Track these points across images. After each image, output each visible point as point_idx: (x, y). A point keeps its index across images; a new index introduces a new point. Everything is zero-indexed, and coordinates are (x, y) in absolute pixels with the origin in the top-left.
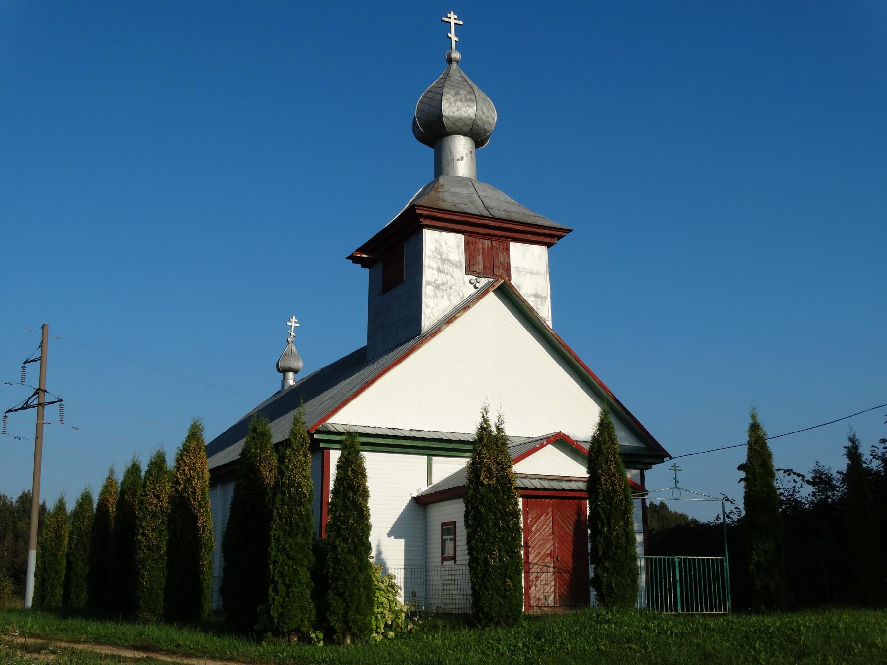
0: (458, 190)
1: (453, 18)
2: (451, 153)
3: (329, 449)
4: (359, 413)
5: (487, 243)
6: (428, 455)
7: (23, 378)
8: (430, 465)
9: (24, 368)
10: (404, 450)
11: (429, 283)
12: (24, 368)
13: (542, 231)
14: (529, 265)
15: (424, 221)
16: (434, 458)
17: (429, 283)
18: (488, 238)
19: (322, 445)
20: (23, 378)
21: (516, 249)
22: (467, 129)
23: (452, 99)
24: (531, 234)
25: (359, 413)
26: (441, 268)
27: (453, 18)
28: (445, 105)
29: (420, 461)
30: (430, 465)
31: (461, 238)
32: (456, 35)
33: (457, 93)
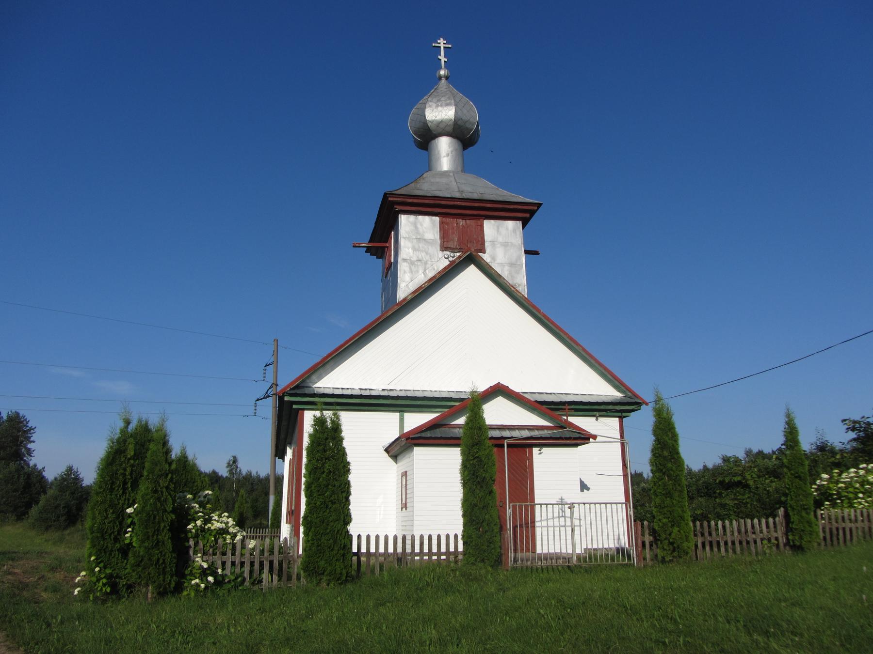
0: (438, 180)
1: (442, 43)
2: (439, 152)
3: (304, 409)
4: (338, 379)
5: (461, 222)
6: (400, 411)
7: (265, 376)
8: (402, 420)
9: (265, 370)
10: (366, 408)
11: (404, 260)
12: (265, 370)
13: (512, 207)
14: (502, 239)
15: (398, 208)
16: (406, 415)
17: (404, 260)
18: (463, 219)
19: (294, 406)
20: (265, 376)
21: (490, 227)
22: (450, 129)
23: (434, 105)
24: (501, 210)
25: (338, 379)
26: (417, 247)
27: (442, 43)
28: (427, 114)
29: (393, 417)
30: (402, 420)
31: (437, 219)
32: (445, 57)
33: (439, 100)
